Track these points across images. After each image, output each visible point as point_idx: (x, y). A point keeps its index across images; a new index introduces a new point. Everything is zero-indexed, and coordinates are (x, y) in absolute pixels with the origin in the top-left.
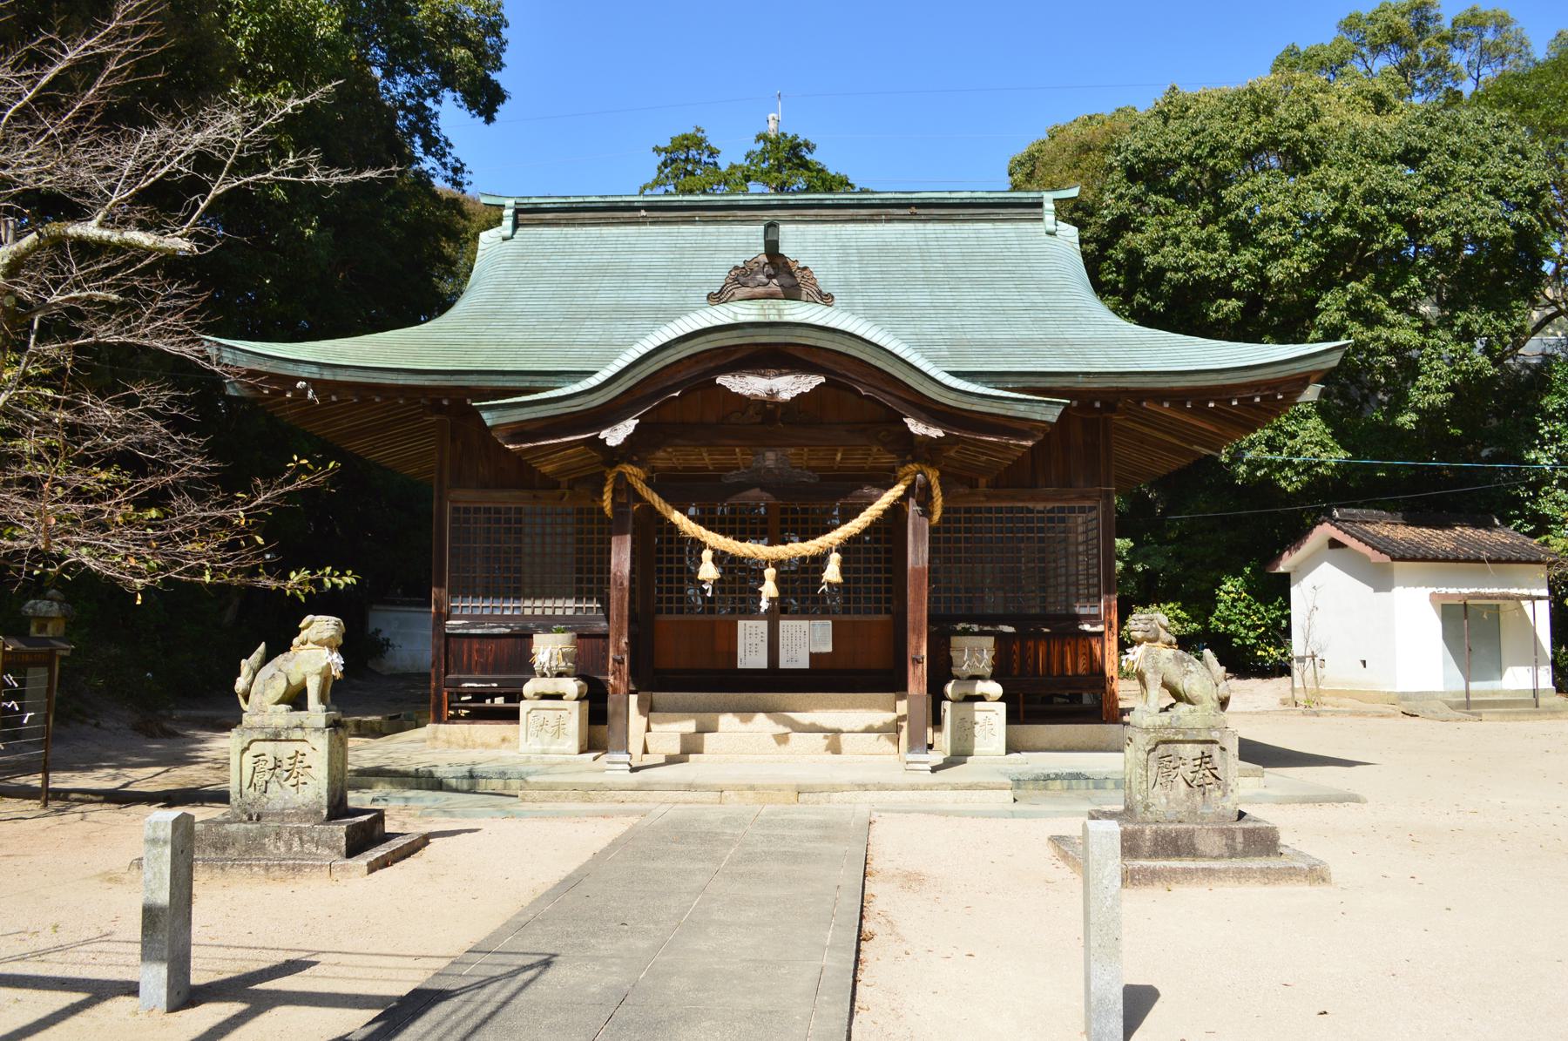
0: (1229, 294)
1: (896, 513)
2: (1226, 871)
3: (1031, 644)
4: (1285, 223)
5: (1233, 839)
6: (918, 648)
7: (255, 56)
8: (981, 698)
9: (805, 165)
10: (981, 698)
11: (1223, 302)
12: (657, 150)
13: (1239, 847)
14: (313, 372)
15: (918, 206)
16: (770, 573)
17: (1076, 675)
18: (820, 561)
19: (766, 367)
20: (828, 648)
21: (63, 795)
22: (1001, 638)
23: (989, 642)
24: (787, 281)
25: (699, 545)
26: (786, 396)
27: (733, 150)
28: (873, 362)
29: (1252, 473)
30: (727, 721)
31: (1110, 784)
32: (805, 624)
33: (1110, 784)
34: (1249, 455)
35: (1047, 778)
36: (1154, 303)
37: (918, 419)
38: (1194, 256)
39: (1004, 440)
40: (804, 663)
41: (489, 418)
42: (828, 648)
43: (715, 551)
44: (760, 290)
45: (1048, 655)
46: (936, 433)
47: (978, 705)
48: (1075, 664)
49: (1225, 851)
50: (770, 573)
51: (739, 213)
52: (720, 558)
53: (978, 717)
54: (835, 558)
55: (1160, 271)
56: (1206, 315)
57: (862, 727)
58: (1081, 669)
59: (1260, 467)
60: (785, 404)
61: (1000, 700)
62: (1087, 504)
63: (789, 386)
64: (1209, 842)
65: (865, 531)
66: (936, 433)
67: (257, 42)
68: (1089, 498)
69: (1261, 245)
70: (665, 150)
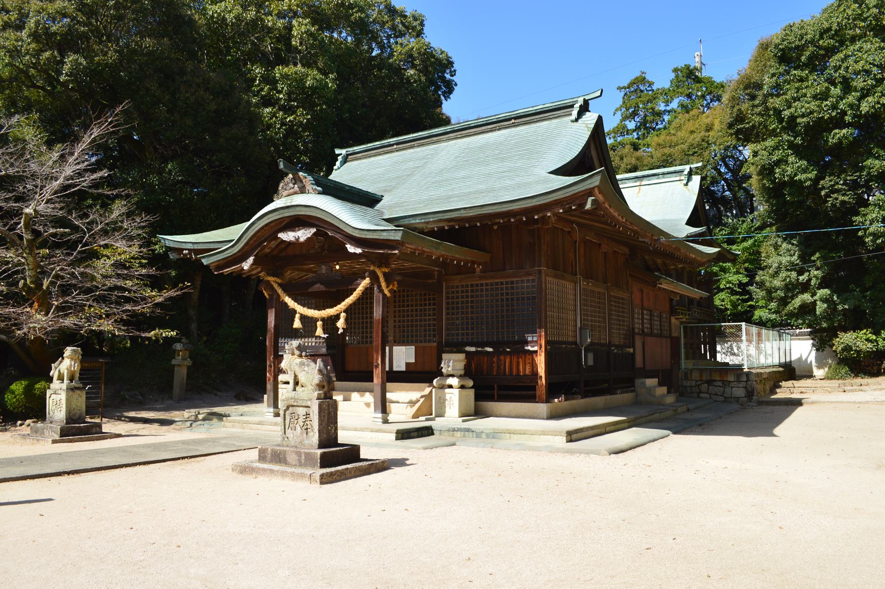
0: (841, 125)
1: (368, 291)
2: (278, 471)
3: (502, 357)
4: (868, 72)
5: (300, 456)
6: (377, 359)
7: (290, 100)
8: (451, 387)
9: (698, 80)
10: (451, 387)
11: (837, 131)
12: (619, 88)
13: (303, 461)
14: (190, 246)
15: (515, 118)
16: (319, 323)
17: (525, 375)
18: (337, 317)
19: (295, 227)
20: (413, 360)
21: (478, 434)
22: (468, 354)
23: (462, 356)
24: (301, 185)
25: (294, 312)
26: (302, 240)
27: (662, 80)
28: (326, 219)
29: (874, 241)
30: (355, 396)
31: (484, 436)
32: (403, 348)
33: (484, 436)
34: (871, 230)
35: (454, 430)
36: (795, 139)
37: (351, 244)
38: (813, 105)
39: (385, 251)
40: (403, 368)
41: (205, 262)
42: (413, 360)
43: (301, 315)
44: (292, 191)
45: (511, 363)
46: (359, 251)
47: (447, 390)
48: (525, 369)
49: (297, 463)
50: (319, 323)
51: (435, 139)
52: (303, 318)
53: (448, 397)
54: (343, 315)
55: (793, 118)
56: (827, 141)
57: (407, 401)
58: (527, 372)
59: (879, 238)
60: (302, 244)
61: (472, 388)
62: (531, 278)
63: (303, 235)
64: (292, 458)
65: (359, 299)
66: (359, 251)
67: (289, 94)
68: (530, 275)
69: (856, 90)
70: (624, 88)
